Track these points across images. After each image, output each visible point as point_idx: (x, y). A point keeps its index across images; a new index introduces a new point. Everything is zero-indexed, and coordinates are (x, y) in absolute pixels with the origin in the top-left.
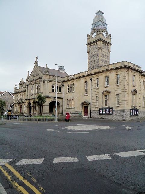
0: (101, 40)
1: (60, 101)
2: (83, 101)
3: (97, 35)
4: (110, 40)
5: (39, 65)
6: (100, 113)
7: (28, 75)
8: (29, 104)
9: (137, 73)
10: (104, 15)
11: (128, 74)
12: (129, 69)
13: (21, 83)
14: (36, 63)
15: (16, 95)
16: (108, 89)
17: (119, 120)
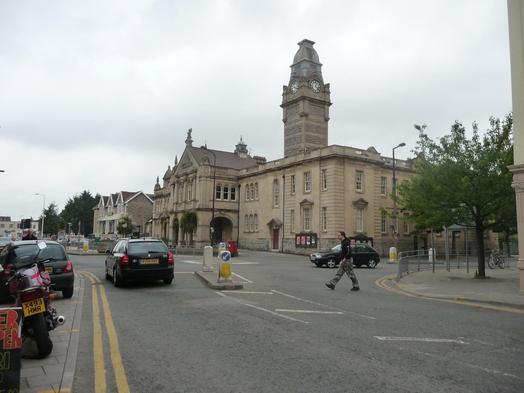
0: (305, 99)
1: (231, 216)
2: (270, 220)
5: (194, 145)
6: (296, 245)
7: (176, 163)
8: (176, 220)
9: (367, 167)
11: (344, 169)
12: (345, 160)
13: (167, 177)
14: (189, 141)
15: (158, 200)
16: (309, 197)
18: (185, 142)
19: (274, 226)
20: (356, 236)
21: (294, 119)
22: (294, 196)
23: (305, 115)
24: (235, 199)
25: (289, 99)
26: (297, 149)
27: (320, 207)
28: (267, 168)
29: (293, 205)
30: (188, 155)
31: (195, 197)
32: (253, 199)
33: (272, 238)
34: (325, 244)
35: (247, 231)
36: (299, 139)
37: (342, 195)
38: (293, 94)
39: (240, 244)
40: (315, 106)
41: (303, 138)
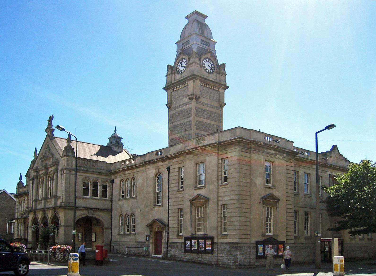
2: (151, 219)
3: (188, 67)
4: (222, 78)
10: (207, 21)
15: (21, 199)
17: (228, 267)
18: (45, 131)
19: (156, 228)
20: (265, 240)
21: (181, 103)
22: (182, 192)
23: (196, 97)
24: (108, 196)
25: (174, 81)
26: (186, 137)
27: (218, 205)
28: (147, 160)
29: (181, 203)
30: (48, 145)
31: (57, 194)
32: (129, 197)
33: (154, 241)
34: (225, 250)
35: (122, 233)
36: (187, 127)
37: (248, 189)
38: (179, 73)
39: (113, 248)
40: (208, 89)
41: (193, 124)
